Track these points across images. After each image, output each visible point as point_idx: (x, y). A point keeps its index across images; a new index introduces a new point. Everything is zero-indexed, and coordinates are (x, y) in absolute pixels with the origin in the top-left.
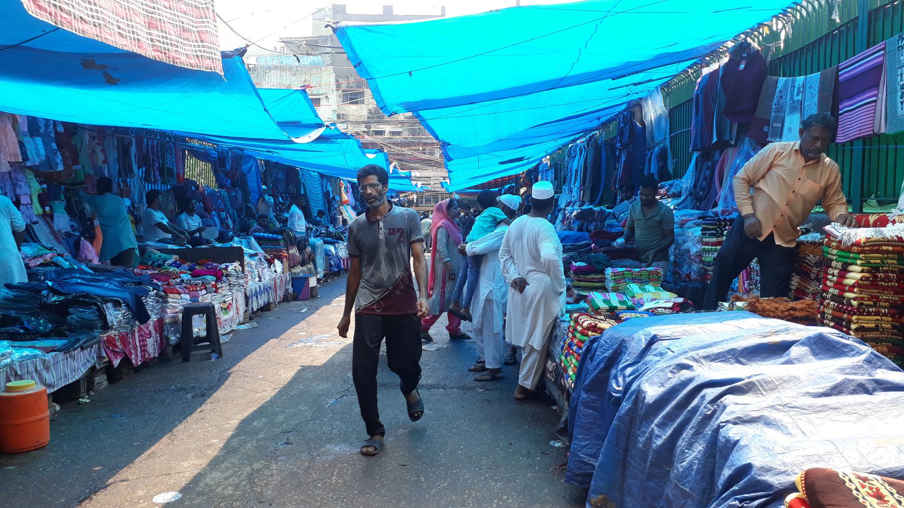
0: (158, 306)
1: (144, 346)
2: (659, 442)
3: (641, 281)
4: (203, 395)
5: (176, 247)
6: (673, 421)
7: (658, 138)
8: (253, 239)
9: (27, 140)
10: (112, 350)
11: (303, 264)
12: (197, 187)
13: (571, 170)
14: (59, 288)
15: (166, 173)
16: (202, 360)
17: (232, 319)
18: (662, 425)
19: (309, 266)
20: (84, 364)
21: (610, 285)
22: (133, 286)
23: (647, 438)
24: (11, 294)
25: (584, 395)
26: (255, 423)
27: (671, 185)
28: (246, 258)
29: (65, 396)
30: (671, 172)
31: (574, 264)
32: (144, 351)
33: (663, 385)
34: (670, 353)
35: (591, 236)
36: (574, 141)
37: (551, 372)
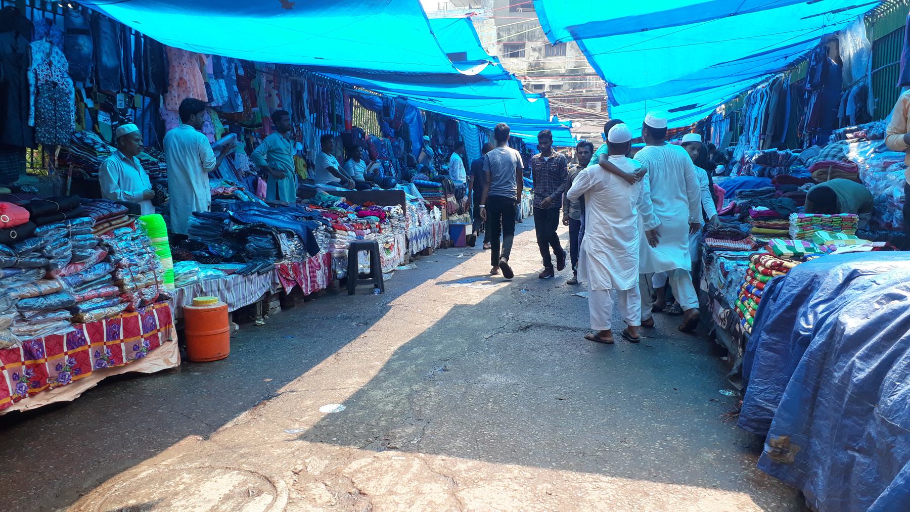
0: (327, 241)
1: (313, 277)
2: (862, 376)
3: (832, 228)
4: (367, 323)
5: (343, 190)
6: (880, 353)
7: (856, 76)
8: (414, 186)
9: (212, 81)
10: (285, 278)
11: (460, 212)
12: (363, 134)
13: (750, 118)
14: (239, 218)
15: (337, 120)
16: (365, 294)
17: (393, 259)
18: (866, 358)
19: (465, 215)
20: (260, 289)
21: (795, 231)
22: (305, 220)
23: (845, 373)
24: (197, 221)
25: (764, 336)
26: (415, 350)
27: (871, 127)
28: (407, 202)
29: (244, 316)
30: (871, 113)
31: (754, 208)
32: (314, 282)
33: (867, 317)
34: (875, 285)
35: (773, 183)
36: (755, 86)
37: (722, 320)
